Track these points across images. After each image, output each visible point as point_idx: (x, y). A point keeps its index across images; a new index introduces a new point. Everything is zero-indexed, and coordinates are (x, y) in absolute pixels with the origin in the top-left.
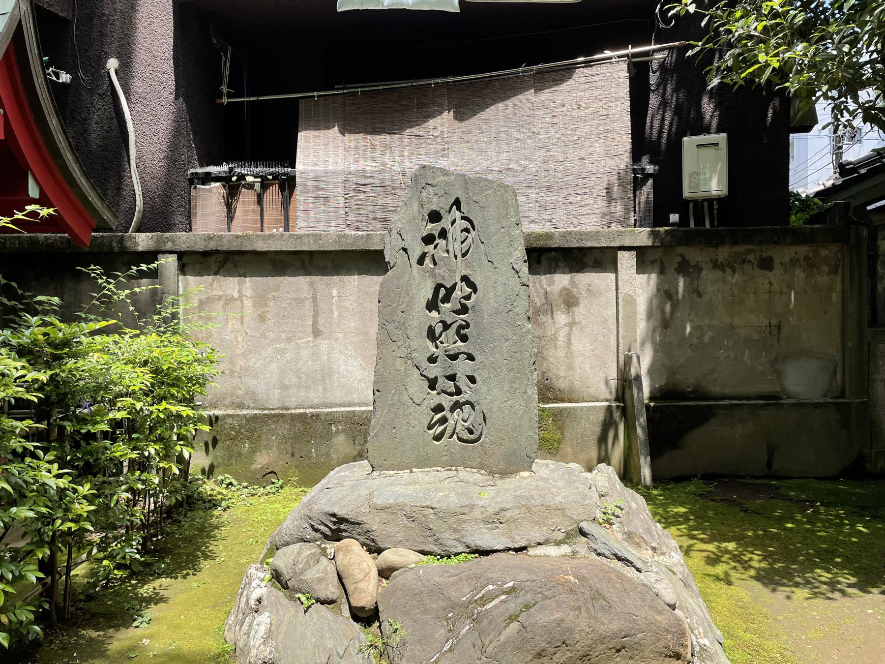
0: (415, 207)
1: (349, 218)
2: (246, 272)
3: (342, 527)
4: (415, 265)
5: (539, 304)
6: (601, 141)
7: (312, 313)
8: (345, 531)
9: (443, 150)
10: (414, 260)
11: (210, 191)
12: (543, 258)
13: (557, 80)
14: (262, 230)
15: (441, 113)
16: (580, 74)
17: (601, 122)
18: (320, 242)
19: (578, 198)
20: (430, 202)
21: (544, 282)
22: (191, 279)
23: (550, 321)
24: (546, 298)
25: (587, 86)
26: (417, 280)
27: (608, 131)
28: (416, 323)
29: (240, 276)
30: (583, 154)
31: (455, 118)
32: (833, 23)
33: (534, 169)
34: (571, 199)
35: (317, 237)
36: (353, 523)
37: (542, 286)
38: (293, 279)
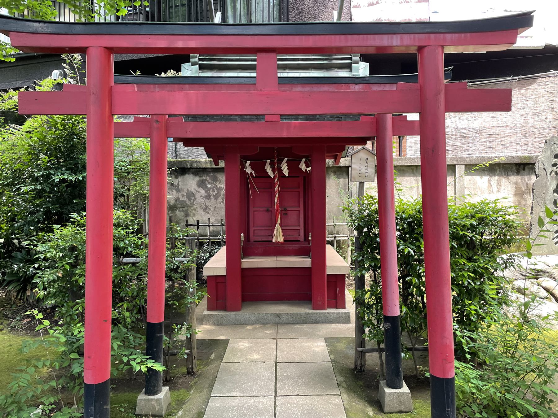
0: (549, 152)
3: (539, 274)
4: (549, 175)
5: (523, 189)
6: (551, 112)
7: (417, 194)
8: (540, 275)
9: (475, 117)
10: (548, 174)
12: (526, 168)
13: (528, 84)
14: (176, 159)
16: (539, 82)
17: (550, 104)
19: (540, 139)
20: (555, 150)
21: (526, 179)
23: (529, 197)
24: (527, 187)
25: (543, 87)
26: (550, 181)
27: (553, 108)
28: (549, 198)
30: (542, 118)
33: (519, 126)
34: (536, 140)
36: (545, 272)
37: (525, 181)
38: (408, 178)
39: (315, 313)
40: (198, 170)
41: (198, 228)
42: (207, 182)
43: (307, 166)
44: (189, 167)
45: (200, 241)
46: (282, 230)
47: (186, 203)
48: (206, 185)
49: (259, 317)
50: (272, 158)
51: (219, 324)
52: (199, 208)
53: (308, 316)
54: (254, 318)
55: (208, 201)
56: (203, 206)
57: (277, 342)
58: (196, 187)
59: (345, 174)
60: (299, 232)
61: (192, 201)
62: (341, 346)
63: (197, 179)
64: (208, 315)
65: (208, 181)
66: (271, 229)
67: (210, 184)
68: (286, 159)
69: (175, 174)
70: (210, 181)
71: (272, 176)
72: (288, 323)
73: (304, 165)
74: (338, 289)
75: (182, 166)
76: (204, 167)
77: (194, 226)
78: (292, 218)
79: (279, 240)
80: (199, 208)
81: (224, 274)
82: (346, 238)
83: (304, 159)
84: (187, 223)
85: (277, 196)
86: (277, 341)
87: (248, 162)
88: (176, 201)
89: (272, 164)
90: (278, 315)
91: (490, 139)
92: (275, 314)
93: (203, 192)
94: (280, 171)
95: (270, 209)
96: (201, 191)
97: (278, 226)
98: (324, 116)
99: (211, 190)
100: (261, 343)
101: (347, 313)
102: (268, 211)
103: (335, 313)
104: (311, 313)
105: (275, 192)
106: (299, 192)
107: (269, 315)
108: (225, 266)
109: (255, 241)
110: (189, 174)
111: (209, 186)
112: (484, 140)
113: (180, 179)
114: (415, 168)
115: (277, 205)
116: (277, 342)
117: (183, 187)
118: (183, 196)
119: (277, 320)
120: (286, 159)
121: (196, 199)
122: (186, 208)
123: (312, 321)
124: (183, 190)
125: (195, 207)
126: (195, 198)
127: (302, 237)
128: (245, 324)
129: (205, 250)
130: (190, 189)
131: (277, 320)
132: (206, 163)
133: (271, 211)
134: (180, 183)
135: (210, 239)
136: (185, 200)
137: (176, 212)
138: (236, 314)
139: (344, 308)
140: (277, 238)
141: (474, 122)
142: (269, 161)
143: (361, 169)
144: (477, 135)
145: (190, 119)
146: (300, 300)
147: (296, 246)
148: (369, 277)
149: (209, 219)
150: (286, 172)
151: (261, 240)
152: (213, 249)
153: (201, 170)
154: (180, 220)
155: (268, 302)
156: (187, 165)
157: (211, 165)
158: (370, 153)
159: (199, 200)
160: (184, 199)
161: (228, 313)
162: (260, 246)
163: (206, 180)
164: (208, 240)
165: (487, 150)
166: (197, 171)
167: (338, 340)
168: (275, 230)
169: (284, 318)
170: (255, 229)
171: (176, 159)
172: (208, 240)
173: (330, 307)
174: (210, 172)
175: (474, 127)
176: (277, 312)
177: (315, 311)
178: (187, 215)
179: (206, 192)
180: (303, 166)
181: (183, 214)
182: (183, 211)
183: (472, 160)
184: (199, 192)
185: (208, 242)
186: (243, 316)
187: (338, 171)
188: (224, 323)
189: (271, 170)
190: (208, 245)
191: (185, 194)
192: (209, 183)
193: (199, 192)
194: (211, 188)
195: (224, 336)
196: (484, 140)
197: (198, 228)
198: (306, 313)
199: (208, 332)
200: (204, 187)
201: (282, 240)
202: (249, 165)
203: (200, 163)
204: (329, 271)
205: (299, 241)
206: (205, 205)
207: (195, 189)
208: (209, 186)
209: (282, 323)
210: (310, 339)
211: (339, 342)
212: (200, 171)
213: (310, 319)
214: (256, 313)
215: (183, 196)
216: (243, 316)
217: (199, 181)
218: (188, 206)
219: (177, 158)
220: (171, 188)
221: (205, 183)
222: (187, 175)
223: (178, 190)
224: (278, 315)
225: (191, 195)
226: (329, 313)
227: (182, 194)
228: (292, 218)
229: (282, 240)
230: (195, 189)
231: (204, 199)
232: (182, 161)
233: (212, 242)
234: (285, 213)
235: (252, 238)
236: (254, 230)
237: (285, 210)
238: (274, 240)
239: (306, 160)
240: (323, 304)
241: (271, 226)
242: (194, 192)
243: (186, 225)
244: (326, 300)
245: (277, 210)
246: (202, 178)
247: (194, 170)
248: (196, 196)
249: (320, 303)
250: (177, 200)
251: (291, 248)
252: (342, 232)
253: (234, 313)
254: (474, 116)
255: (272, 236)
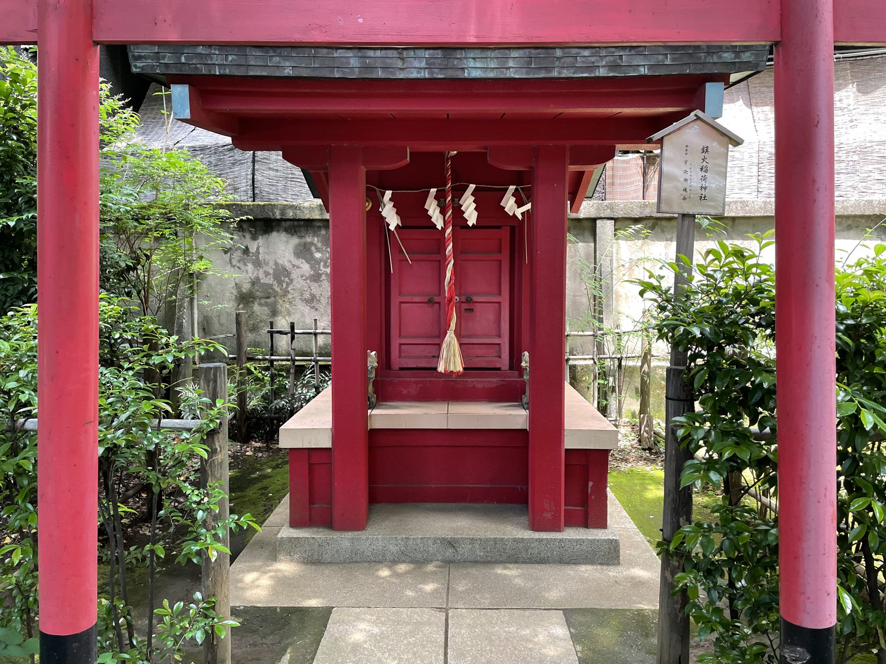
1: (762, 186)
2: (672, 237)
11: (627, 162)
14: (254, 201)
15: (846, 86)
18: (747, 208)
22: (622, 243)
29: (667, 240)
31: (859, 91)
32: (846, 534)
35: (744, 203)
39: (537, 540)
40: (296, 223)
41: (293, 338)
42: (313, 248)
43: (520, 203)
44: (278, 217)
45: (297, 363)
46: (461, 345)
47: (273, 289)
48: (312, 254)
49: (406, 546)
50: (440, 183)
51: (314, 560)
52: (297, 300)
53: (521, 545)
54: (393, 548)
55: (316, 285)
56: (307, 296)
57: (447, 620)
58: (292, 258)
59: (587, 234)
60: (500, 351)
61: (285, 285)
62: (607, 636)
63: (295, 241)
64: (290, 540)
65: (315, 245)
66: (437, 341)
67: (319, 252)
68: (472, 186)
69: (250, 232)
70: (319, 245)
71: (439, 225)
72: (475, 562)
73: (512, 200)
74: (591, 484)
75: (265, 216)
76: (307, 217)
77: (286, 334)
78: (484, 318)
79: (452, 369)
80: (297, 300)
81: (328, 444)
82: (591, 362)
83: (512, 188)
84: (272, 328)
85: (450, 266)
86: (447, 615)
87: (388, 194)
88: (253, 284)
89: (439, 197)
90: (451, 543)
91: (880, 166)
92: (444, 539)
93: (306, 268)
94: (458, 213)
95: (436, 299)
96: (302, 266)
97: (451, 338)
98: (574, 51)
99: (322, 264)
100: (409, 624)
101: (611, 541)
102: (430, 302)
103: (583, 541)
104: (529, 539)
105: (445, 258)
106: (500, 261)
107: (430, 542)
108: (329, 425)
109: (401, 369)
110: (278, 231)
111: (318, 255)
112: (870, 167)
113: (261, 240)
114: (730, 223)
115: (450, 288)
116: (447, 620)
117: (267, 257)
118: (267, 274)
119: (449, 553)
120: (472, 186)
121: (292, 280)
122: (272, 299)
123: (530, 559)
124: (267, 264)
125: (290, 296)
126: (290, 279)
127: (504, 361)
128: (375, 562)
129: (308, 382)
130: (280, 262)
131: (449, 553)
132: (311, 209)
133: (439, 303)
134: (261, 250)
135: (316, 361)
136: (271, 282)
137: (252, 307)
138: (353, 539)
139: (604, 526)
140: (447, 362)
141: (849, 130)
142: (433, 191)
143: (687, 176)
144: (856, 158)
145: (230, 58)
146: (500, 501)
147: (493, 381)
148: (636, 441)
149: (315, 320)
150: (471, 216)
151: (414, 366)
152: (325, 381)
153: (302, 223)
154: (261, 321)
155: (427, 505)
156: (274, 214)
157: (322, 214)
158: (714, 131)
159: (299, 283)
160: (270, 280)
161: (336, 535)
162: (412, 379)
163: (312, 244)
164: (313, 363)
165: (876, 187)
166: (294, 227)
167: (598, 615)
168: (444, 345)
169: (464, 550)
170: (404, 341)
171: (254, 201)
172: (313, 363)
173: (572, 521)
174: (319, 227)
175: (851, 142)
176: (450, 535)
177: (537, 535)
178: (274, 313)
179: (311, 268)
180: (509, 204)
181: (266, 310)
182: (266, 304)
183: (847, 207)
184: (298, 267)
185: (313, 366)
186: (369, 542)
187: (574, 228)
188: (327, 557)
189: (438, 210)
190: (313, 372)
191: (271, 272)
192: (318, 250)
193: (298, 267)
194: (321, 260)
195: (315, 597)
196: (870, 167)
197: (293, 338)
198: (515, 540)
199: (283, 582)
200: (308, 256)
201: (459, 368)
202: (391, 200)
203: (300, 209)
204: (570, 443)
205: (499, 369)
206: (311, 294)
207: (290, 262)
208: (318, 255)
209: (459, 561)
210: (527, 613)
211: (601, 625)
212: (299, 226)
213: (524, 553)
214: (399, 537)
215: (267, 274)
216: (369, 542)
217: (299, 245)
218: (276, 295)
219: (257, 200)
220: (243, 259)
221: (309, 249)
222: (275, 234)
223: (258, 264)
224: (450, 543)
225: (281, 273)
226: (569, 540)
227: (265, 272)
228: (484, 318)
229: (457, 366)
230: (290, 262)
231: (308, 281)
232: (264, 205)
233: (320, 366)
234: (467, 308)
235: (397, 361)
236: (401, 344)
237: (469, 301)
238: (441, 368)
239: (516, 190)
240: (556, 518)
241: (439, 336)
242: (288, 266)
243: (269, 332)
244: (563, 507)
245: (450, 300)
246: (303, 240)
247: (288, 223)
248: (293, 276)
249: (548, 515)
250: (254, 282)
251: (480, 386)
252: (580, 350)
253: (349, 535)
254: (849, 119)
255: (437, 357)
